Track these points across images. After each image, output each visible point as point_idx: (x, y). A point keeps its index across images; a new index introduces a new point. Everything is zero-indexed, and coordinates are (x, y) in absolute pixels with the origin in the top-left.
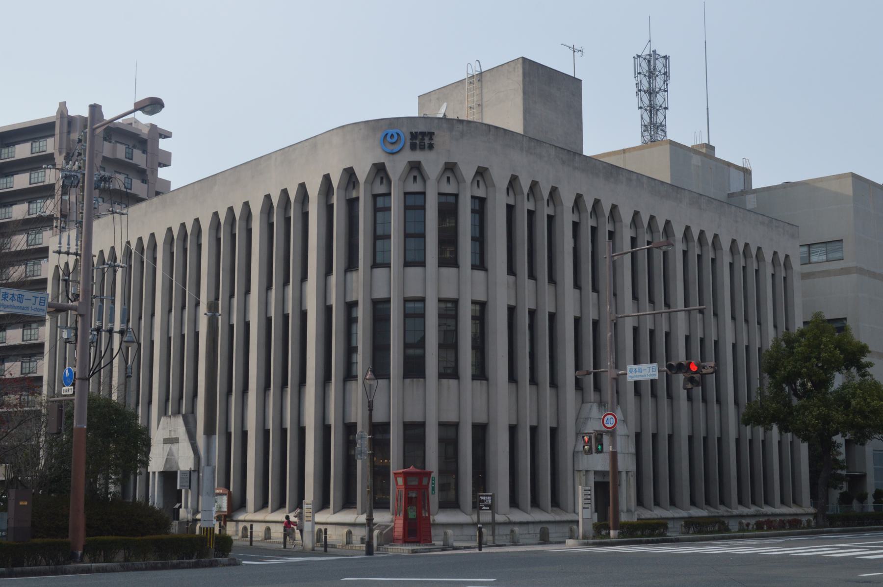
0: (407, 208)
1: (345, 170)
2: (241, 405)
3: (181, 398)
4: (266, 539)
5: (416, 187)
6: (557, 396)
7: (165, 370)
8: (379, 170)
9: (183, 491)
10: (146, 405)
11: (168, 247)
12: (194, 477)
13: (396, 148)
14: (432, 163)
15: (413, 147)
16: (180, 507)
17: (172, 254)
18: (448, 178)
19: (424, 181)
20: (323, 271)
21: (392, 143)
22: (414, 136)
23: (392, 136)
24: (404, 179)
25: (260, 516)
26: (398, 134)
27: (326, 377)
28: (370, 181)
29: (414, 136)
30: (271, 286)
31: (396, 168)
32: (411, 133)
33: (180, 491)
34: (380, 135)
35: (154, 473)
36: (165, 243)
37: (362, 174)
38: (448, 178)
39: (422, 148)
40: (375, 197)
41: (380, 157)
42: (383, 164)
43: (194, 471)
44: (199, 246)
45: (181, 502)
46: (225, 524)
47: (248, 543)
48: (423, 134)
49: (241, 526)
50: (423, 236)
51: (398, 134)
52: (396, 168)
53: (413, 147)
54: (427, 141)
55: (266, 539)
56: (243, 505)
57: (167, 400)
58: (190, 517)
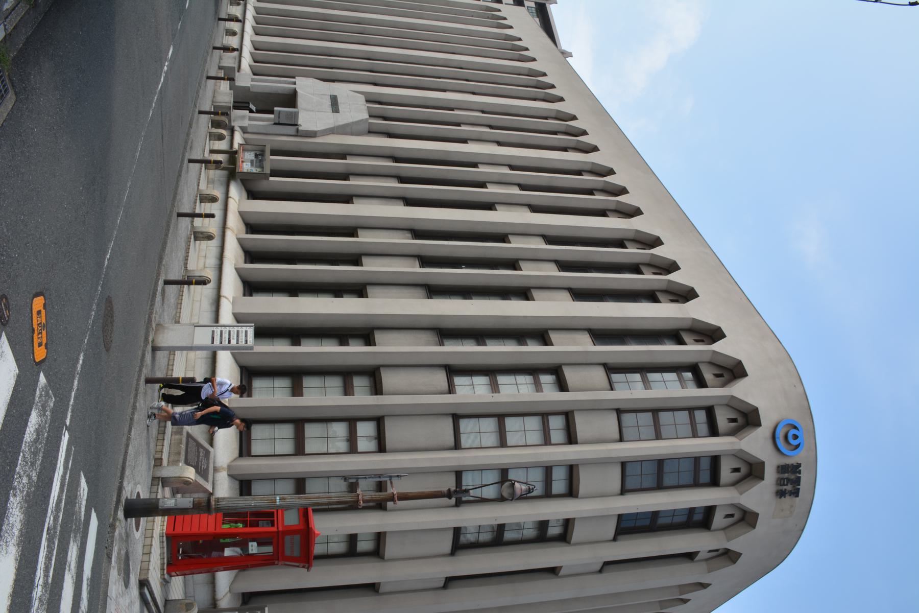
0: (697, 460)
1: (739, 363)
2: (387, 194)
3: (385, 119)
4: (195, 233)
5: (726, 474)
6: (214, 97)
7: (440, 104)
8: (748, 418)
9: (272, 116)
10: (373, 81)
11: (553, 115)
12: (292, 130)
13: (781, 443)
14: (758, 497)
15: (782, 469)
16: (251, 111)
17: (546, 118)
18: (732, 516)
19: (734, 484)
20: (418, 226)
21: (786, 437)
22: (796, 468)
23: (796, 437)
24: (739, 455)
25: (234, 221)
26: (798, 446)
27: (446, 332)
28: (733, 404)
29: (796, 468)
30: (402, 182)
31: (755, 444)
32: (799, 465)
33: (272, 112)
34: (795, 418)
35: (295, 83)
36: (558, 111)
37: (740, 390)
38: (732, 516)
39: (780, 482)
40: (710, 411)
41: (768, 419)
42: (759, 425)
43: (298, 130)
44: (565, 149)
45: (258, 112)
46: (224, 169)
47: (186, 209)
48: (798, 481)
49: (218, 193)
50: (659, 486)
51: (798, 446)
52: (755, 444)
53: (782, 469)
54: (789, 487)
55: (195, 233)
56: (253, 195)
57: (381, 103)
58: (236, 124)
